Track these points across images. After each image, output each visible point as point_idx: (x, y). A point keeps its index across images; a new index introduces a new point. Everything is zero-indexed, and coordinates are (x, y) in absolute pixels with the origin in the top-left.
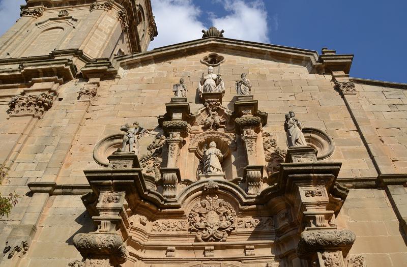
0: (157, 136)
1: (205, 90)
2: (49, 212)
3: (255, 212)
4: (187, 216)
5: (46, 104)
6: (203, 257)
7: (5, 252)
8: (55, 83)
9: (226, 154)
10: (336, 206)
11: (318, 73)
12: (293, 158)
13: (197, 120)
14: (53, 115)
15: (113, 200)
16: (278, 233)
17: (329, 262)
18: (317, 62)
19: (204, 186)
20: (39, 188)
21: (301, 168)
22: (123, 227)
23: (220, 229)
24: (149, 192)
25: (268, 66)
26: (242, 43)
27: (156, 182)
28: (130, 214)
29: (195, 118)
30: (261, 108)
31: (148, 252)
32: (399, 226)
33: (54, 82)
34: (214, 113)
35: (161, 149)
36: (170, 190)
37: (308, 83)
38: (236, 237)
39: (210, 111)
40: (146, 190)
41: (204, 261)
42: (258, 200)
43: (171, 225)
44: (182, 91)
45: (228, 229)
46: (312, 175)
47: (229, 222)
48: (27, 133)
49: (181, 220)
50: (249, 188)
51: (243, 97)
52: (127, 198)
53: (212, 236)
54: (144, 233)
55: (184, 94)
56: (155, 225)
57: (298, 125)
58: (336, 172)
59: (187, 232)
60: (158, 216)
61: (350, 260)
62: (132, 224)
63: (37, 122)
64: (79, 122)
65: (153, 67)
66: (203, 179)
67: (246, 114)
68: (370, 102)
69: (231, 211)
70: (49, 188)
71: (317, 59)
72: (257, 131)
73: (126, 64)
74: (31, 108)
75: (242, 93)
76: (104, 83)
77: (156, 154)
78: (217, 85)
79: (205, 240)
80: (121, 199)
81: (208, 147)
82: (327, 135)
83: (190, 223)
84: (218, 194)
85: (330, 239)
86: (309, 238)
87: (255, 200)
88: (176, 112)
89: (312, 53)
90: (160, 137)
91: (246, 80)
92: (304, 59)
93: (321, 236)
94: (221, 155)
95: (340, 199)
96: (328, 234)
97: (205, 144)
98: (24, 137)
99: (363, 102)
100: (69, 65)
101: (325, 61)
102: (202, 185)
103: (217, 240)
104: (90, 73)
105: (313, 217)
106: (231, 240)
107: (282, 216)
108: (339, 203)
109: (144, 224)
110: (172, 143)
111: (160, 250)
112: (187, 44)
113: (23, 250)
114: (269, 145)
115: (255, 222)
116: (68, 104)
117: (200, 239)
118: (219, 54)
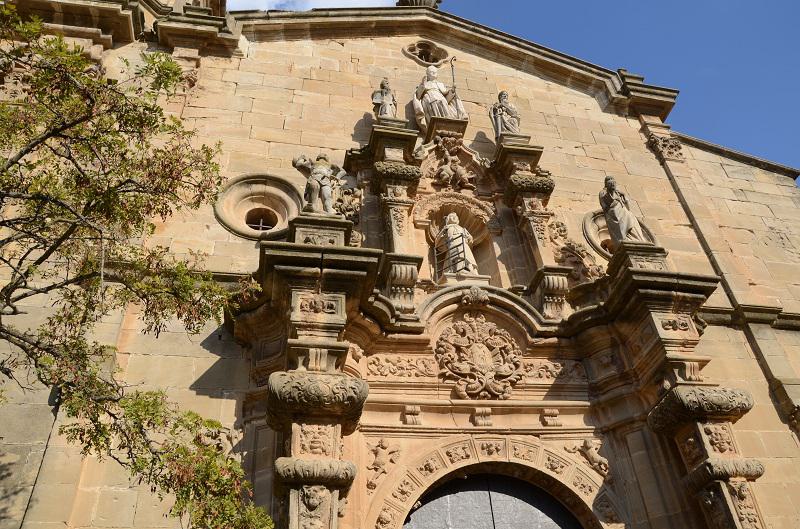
3: (552, 350)
8: (95, 43)
11: (617, 113)
16: (593, 391)
18: (618, 93)
19: (463, 295)
21: (660, 280)
25: (530, 84)
26: (483, 30)
32: (768, 390)
33: (91, 41)
34: (453, 158)
35: (356, 215)
37: (603, 128)
38: (523, 393)
42: (562, 330)
45: (512, 378)
46: (674, 293)
49: (422, 356)
60: (378, 346)
65: (307, 46)
68: (705, 180)
71: (619, 88)
73: (252, 29)
75: (508, 129)
79: (473, 396)
84: (486, 312)
85: (719, 402)
87: (556, 328)
88: (391, 147)
89: (610, 75)
92: (593, 82)
97: (439, 217)
99: (695, 178)
100: (131, 8)
101: (632, 93)
102: (460, 293)
103: (495, 397)
105: (303, 351)
106: (516, 398)
112: (377, 12)
115: (555, 367)
118: (439, 45)
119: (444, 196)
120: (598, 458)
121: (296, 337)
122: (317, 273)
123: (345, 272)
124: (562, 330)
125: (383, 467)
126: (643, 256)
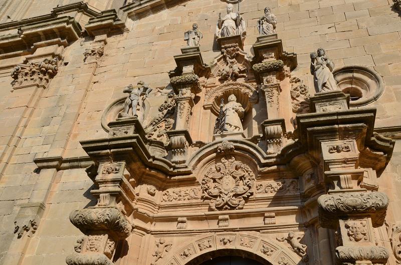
0: (169, 94)
1: (222, 34)
2: (57, 188)
4: (201, 183)
5: (50, 71)
6: (216, 227)
7: (15, 233)
8: (59, 46)
9: (247, 108)
10: (377, 162)
12: (317, 107)
13: (213, 71)
14: (59, 82)
15: (113, 170)
17: (352, 232)
19: (218, 147)
20: (45, 164)
21: (322, 119)
22: (124, 198)
23: (236, 195)
24: (154, 159)
27: (165, 147)
28: (135, 185)
29: (209, 70)
30: (287, 49)
31: (158, 224)
36: (179, 154)
39: (228, 58)
40: (149, 157)
41: (218, 232)
43: (183, 194)
44: (194, 39)
45: (245, 196)
46: (336, 126)
47: (246, 187)
48: (32, 105)
49: (193, 187)
50: (268, 146)
51: (264, 37)
52: (128, 166)
53: (227, 203)
54: (154, 205)
55: (197, 43)
56: (166, 194)
57: (328, 65)
58: (370, 121)
59: (200, 201)
61: (395, 229)
62: (138, 195)
63: (42, 92)
64: (86, 87)
66: (218, 139)
67: (268, 58)
69: (249, 174)
70: (55, 163)
72: (281, 77)
73: (134, 14)
74: (35, 77)
76: (112, 40)
77: (167, 116)
78: (237, 26)
79: (220, 209)
80: (121, 169)
81: (226, 102)
82: (375, 72)
83: (203, 190)
84: (235, 155)
85: (354, 204)
86: (327, 203)
87: (275, 160)
90: (172, 95)
91: (270, 16)
93: (342, 201)
94: (242, 110)
95: (382, 153)
96: (352, 198)
98: (30, 110)
100: (71, 23)
102: (216, 146)
103: (233, 208)
104: (96, 30)
105: (337, 177)
106: (249, 208)
107: (307, 177)
108: (382, 158)
109: (153, 195)
110: (181, 102)
111: (172, 221)
113: (32, 229)
114: (299, 92)
115: (276, 185)
116: (75, 68)
117: (214, 207)
119: (225, 86)
120: (300, 246)
121: (329, 170)
122: (108, 153)
123: (121, 149)
124: (279, 160)
125: (160, 254)
126: (326, 102)
